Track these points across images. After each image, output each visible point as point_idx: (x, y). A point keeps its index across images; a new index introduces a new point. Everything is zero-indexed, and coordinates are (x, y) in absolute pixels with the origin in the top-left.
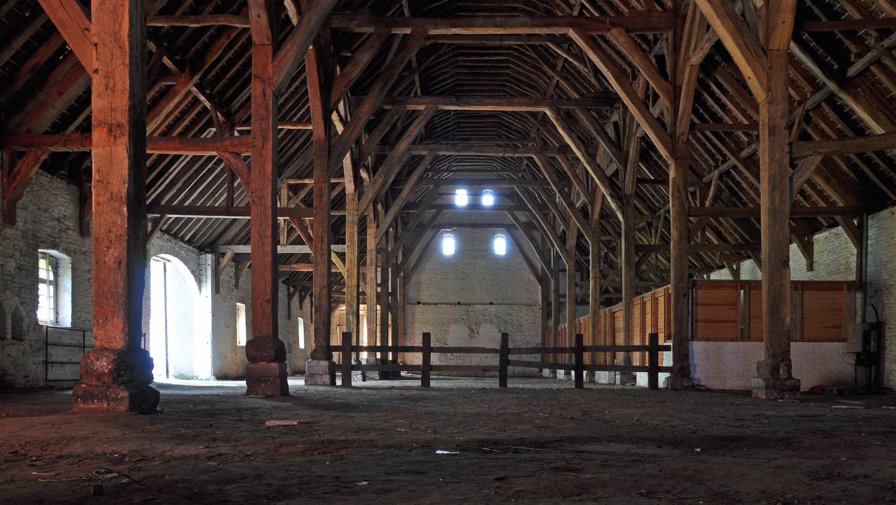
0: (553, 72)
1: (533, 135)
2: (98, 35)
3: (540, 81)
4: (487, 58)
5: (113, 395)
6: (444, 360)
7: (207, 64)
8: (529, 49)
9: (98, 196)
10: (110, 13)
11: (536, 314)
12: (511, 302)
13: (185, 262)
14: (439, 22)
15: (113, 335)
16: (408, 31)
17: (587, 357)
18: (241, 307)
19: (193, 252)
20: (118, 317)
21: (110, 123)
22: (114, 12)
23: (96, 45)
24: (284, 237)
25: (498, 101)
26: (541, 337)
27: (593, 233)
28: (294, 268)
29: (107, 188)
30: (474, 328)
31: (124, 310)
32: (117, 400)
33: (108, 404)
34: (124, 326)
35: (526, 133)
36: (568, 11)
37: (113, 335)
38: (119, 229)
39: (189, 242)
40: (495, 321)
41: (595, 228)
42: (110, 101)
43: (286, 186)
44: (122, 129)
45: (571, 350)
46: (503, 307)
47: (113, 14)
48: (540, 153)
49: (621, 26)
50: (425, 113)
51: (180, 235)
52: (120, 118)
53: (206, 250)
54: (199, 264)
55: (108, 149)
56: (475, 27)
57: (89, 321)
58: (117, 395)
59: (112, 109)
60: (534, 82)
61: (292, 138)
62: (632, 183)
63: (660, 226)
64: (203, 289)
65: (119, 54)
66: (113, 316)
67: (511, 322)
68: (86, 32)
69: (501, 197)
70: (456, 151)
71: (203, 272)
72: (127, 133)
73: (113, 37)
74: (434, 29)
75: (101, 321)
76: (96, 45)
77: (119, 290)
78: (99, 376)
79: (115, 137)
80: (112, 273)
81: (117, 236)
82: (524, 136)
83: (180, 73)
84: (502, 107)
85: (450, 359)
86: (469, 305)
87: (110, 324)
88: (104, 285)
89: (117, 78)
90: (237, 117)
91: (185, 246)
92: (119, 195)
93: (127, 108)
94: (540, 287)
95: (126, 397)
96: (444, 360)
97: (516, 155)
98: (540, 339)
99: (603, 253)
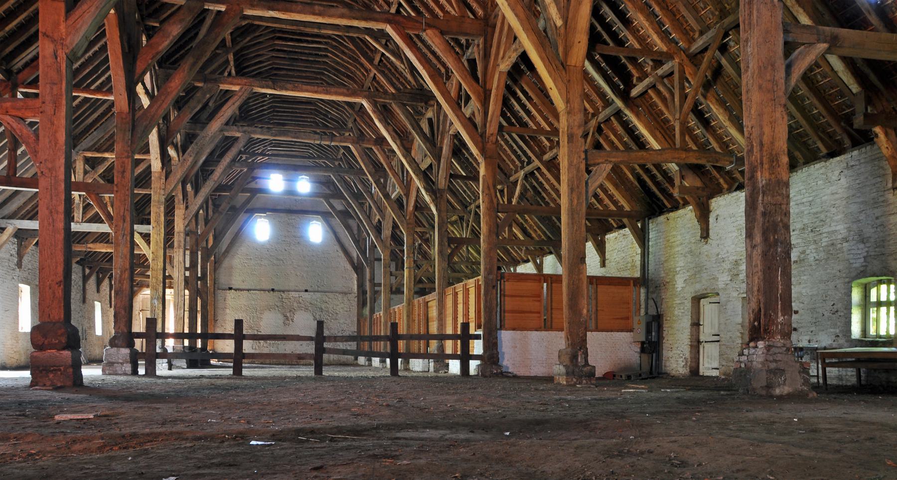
1: (350, 125)
4: (305, 45)
12: (326, 290)
17: (402, 345)
27: (408, 224)
28: (90, 248)
35: (343, 122)
40: (310, 308)
41: (410, 219)
46: (318, 295)
50: (240, 94)
85: (263, 346)
86: (283, 291)
97: (333, 144)
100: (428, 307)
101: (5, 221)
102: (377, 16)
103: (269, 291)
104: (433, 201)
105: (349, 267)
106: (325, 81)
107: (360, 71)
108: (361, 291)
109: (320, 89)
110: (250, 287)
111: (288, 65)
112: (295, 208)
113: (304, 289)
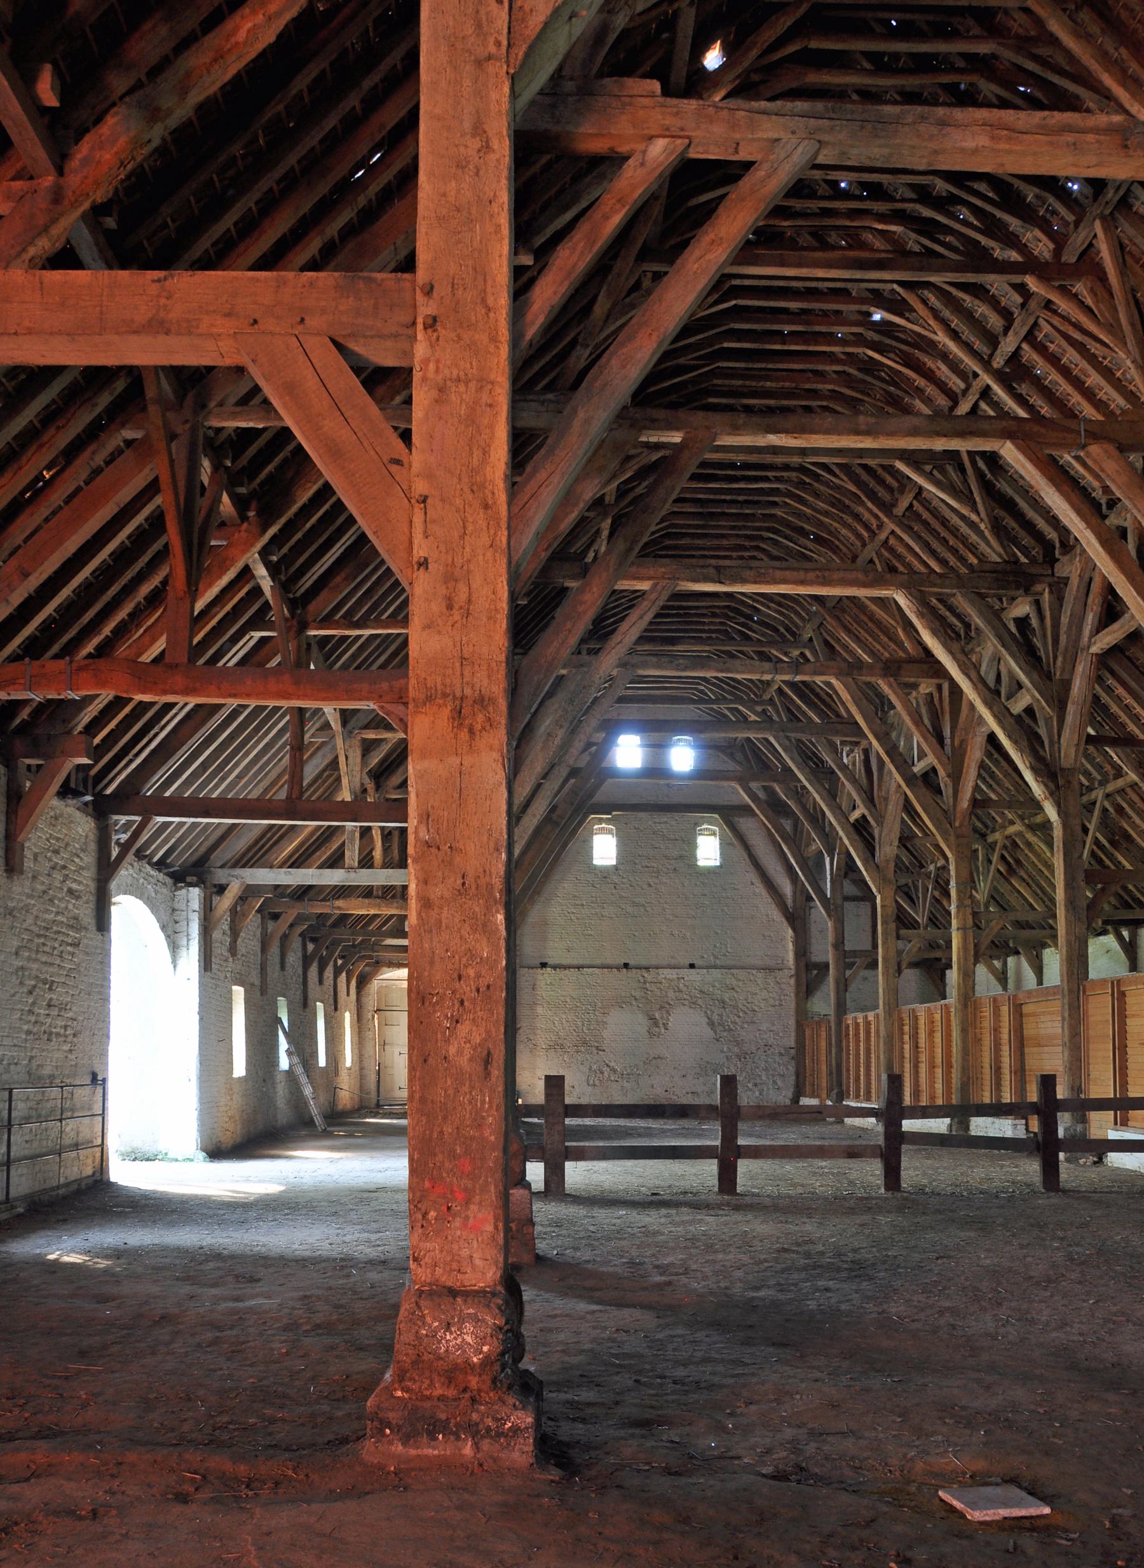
0: (887, 516)
1: (808, 634)
2: (429, 476)
3: (844, 531)
4: (742, 485)
5: (489, 1422)
6: (597, 1083)
7: (295, 502)
8: (837, 471)
9: (426, 882)
10: (460, 422)
11: (783, 986)
12: (730, 963)
13: (154, 909)
14: (741, 421)
15: (465, 1253)
16: (676, 438)
17: (1064, 1125)
18: (238, 992)
19: (165, 884)
20: (480, 1203)
21: (458, 694)
22: (471, 420)
23: (424, 500)
24: (353, 851)
25: (801, 575)
26: (793, 1034)
27: (958, 837)
28: (339, 908)
29: (451, 863)
30: (657, 1015)
31: (496, 1186)
32: (499, 1435)
33: (477, 1447)
34: (496, 1227)
35: (788, 629)
36: (942, 401)
37: (465, 1253)
38: (483, 972)
39: (161, 865)
40: (700, 1002)
41: (961, 825)
42: (458, 639)
43: (358, 743)
44: (491, 709)
45: (1034, 1108)
46: (716, 973)
47: (467, 426)
48: (848, 674)
49: (1110, 440)
50: (653, 596)
51: (148, 852)
52: (485, 682)
53: (189, 879)
54: (174, 910)
55: (454, 761)
56: (815, 433)
57: (16, 1064)
58: (500, 1421)
59: (462, 658)
60: (830, 533)
61: (378, 646)
62: (1078, 745)
63: (1091, 827)
64: (181, 962)
65: (482, 523)
66: (468, 1202)
67: (733, 1003)
68: (394, 468)
69: (709, 751)
70: (678, 670)
71: (182, 926)
72: (503, 722)
73: (465, 480)
74: (729, 434)
75: (432, 1214)
76: (424, 500)
77: (487, 1133)
78: (454, 1372)
79: (471, 731)
80: (466, 1089)
81: (478, 990)
82: (787, 636)
83: (239, 522)
84: (809, 588)
85: (609, 1079)
86: (647, 968)
87: (458, 1222)
88: (445, 1118)
89: (477, 581)
90: (312, 607)
91: (152, 873)
92: (482, 881)
93: (503, 657)
94: (790, 931)
95: (527, 1428)
96: (597, 1083)
97: (798, 678)
98: (793, 1039)
99: (932, 868)
100: (1021, 1015)
101: (226, 871)
102: (985, 426)
103: (618, 968)
104: (1052, 794)
105: (777, 915)
106: (764, 550)
107: (849, 527)
108: (802, 964)
109: (811, 575)
110: (581, 962)
111: (697, 527)
112: (666, 801)
113: (687, 963)
